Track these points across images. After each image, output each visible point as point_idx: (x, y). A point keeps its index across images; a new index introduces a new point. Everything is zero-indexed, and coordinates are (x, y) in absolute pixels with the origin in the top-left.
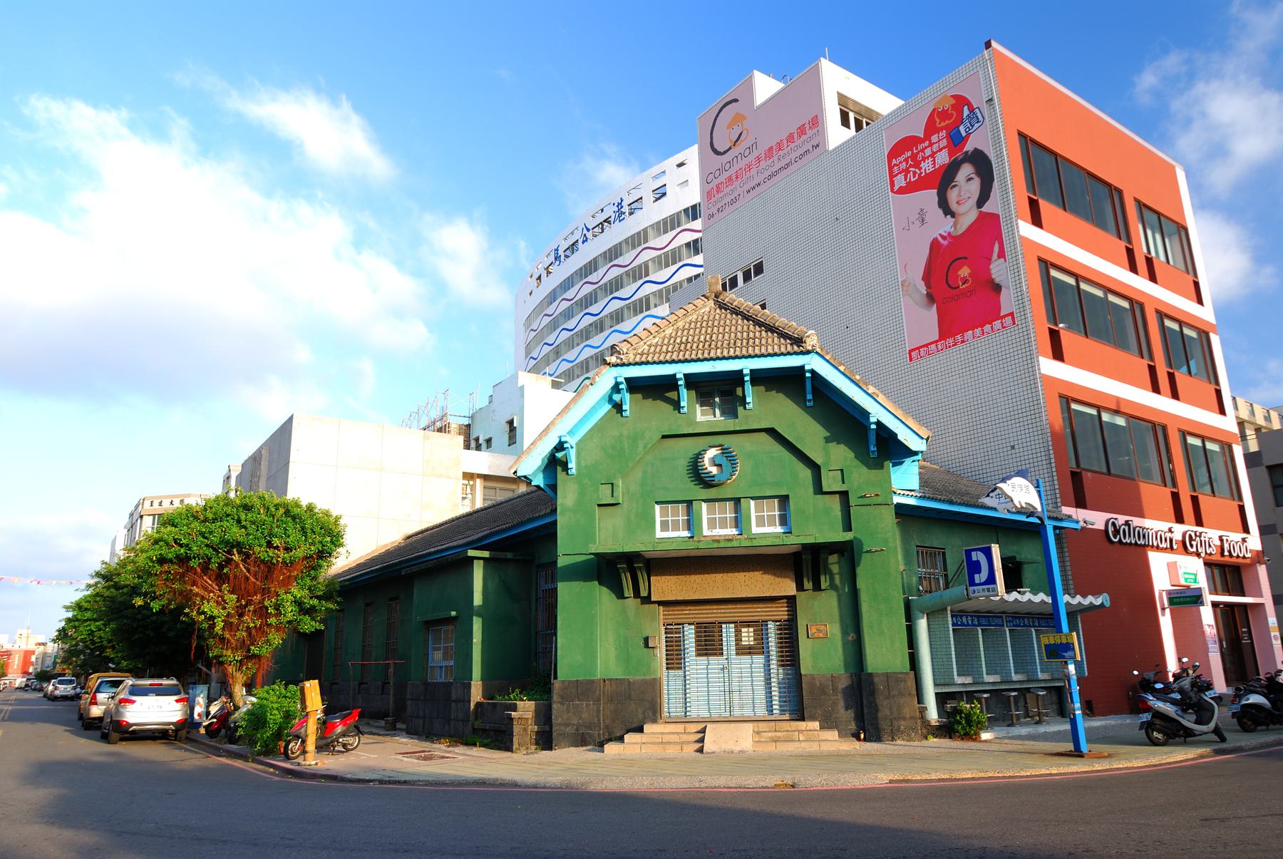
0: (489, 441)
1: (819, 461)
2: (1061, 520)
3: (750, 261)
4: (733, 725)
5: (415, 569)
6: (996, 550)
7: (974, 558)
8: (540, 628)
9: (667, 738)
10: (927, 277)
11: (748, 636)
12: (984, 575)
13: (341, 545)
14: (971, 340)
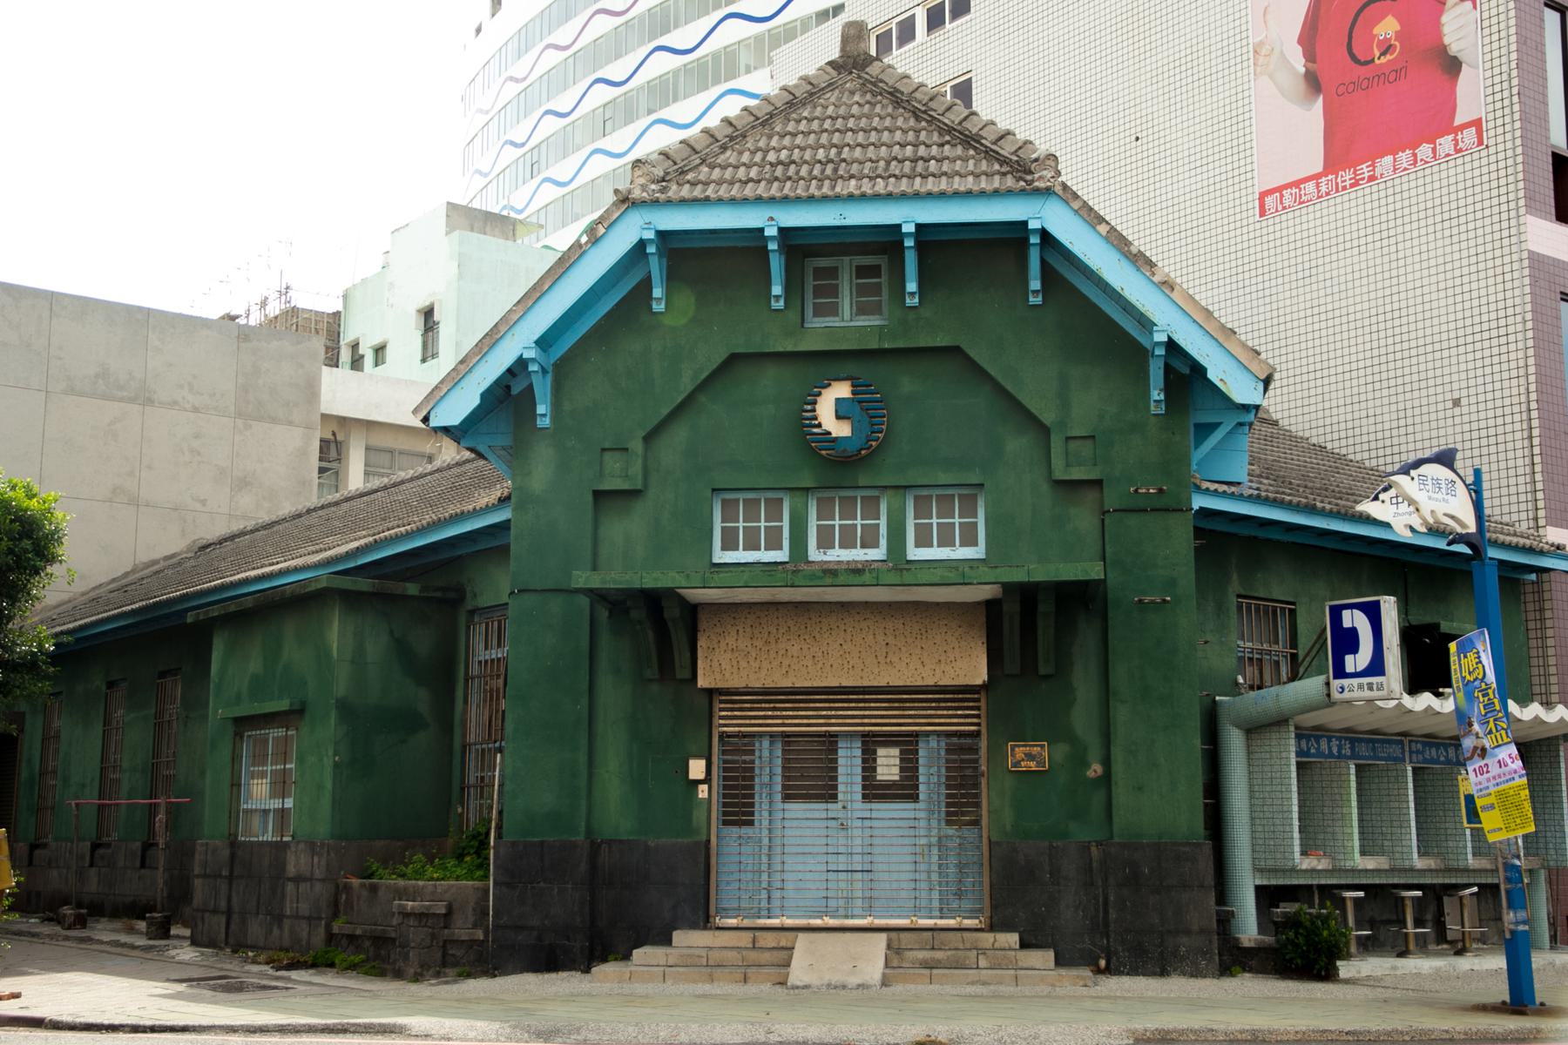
0: (380, 351)
1: (1048, 418)
2: (1542, 553)
5: (215, 612)
6: (1389, 607)
7: (1347, 624)
8: (472, 738)
9: (715, 956)
10: (1309, 38)
11: (888, 765)
13: (52, 559)
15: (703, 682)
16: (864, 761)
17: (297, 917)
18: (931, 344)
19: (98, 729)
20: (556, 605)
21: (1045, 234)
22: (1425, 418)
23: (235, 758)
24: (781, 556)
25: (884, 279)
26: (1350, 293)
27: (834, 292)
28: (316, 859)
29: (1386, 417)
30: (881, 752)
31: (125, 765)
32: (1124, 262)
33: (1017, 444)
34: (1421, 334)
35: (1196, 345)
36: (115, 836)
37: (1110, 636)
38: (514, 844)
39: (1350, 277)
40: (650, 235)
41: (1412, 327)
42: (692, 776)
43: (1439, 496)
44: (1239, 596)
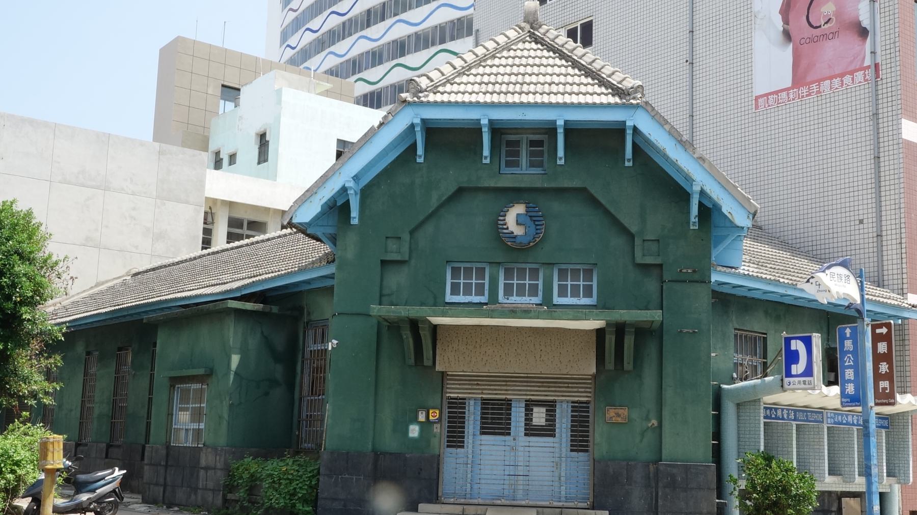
0: (232, 158)
1: (633, 229)
4: (515, 509)
6: (817, 340)
7: (793, 348)
11: (539, 416)
14: (827, 91)
15: (439, 368)
16: (526, 415)
17: (206, 489)
18: (570, 185)
19: (81, 377)
21: (635, 129)
22: (844, 229)
24: (483, 299)
25: (545, 148)
26: (805, 156)
27: (517, 154)
28: (218, 458)
29: (822, 228)
30: (536, 409)
31: (97, 399)
32: (678, 146)
33: (617, 242)
34: (843, 181)
35: (716, 193)
36: (89, 439)
37: (664, 349)
38: (332, 453)
39: (804, 147)
40: (417, 121)
41: (838, 178)
43: (841, 284)
44: (735, 329)
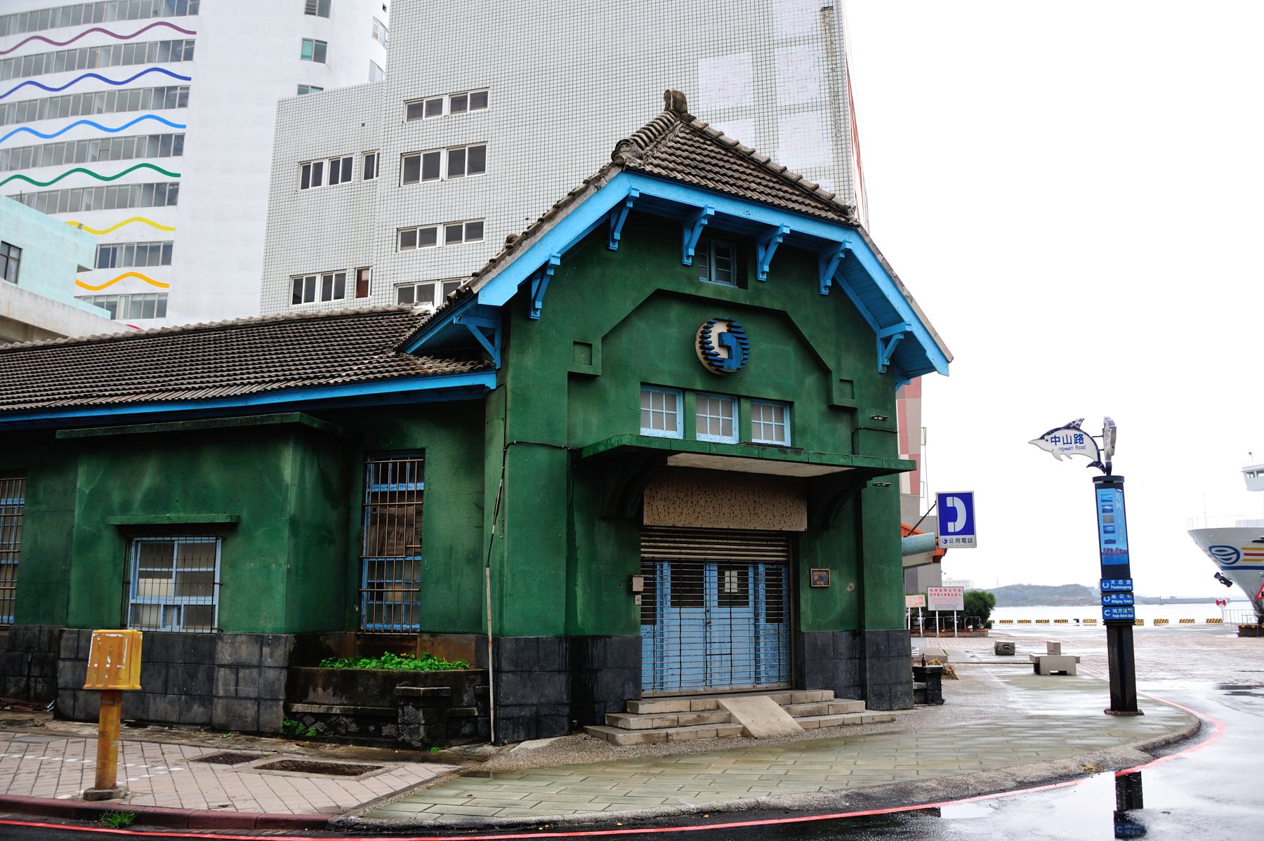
1: (831, 364)
3: (468, 85)
7: (949, 504)
11: (732, 582)
12: (960, 523)
20: (542, 456)
23: (126, 563)
42: (635, 589)
